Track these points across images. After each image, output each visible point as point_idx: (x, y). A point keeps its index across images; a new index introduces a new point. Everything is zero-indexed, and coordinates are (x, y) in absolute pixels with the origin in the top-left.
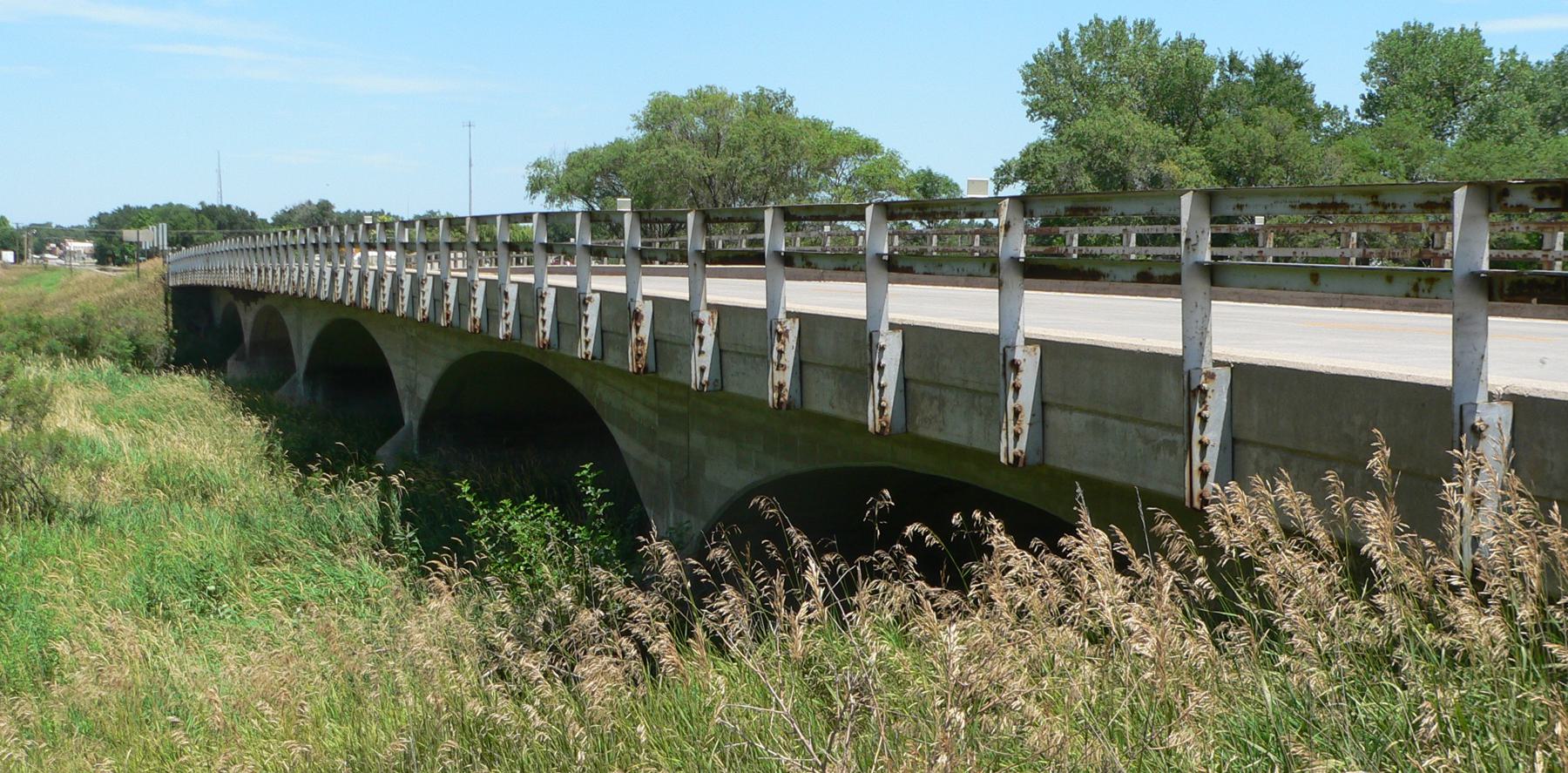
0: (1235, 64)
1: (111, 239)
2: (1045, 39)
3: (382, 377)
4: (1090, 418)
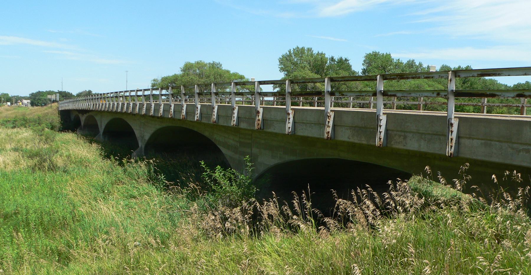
0: (332, 59)
1: (37, 99)
2: (285, 52)
3: (131, 133)
4: (483, 141)
